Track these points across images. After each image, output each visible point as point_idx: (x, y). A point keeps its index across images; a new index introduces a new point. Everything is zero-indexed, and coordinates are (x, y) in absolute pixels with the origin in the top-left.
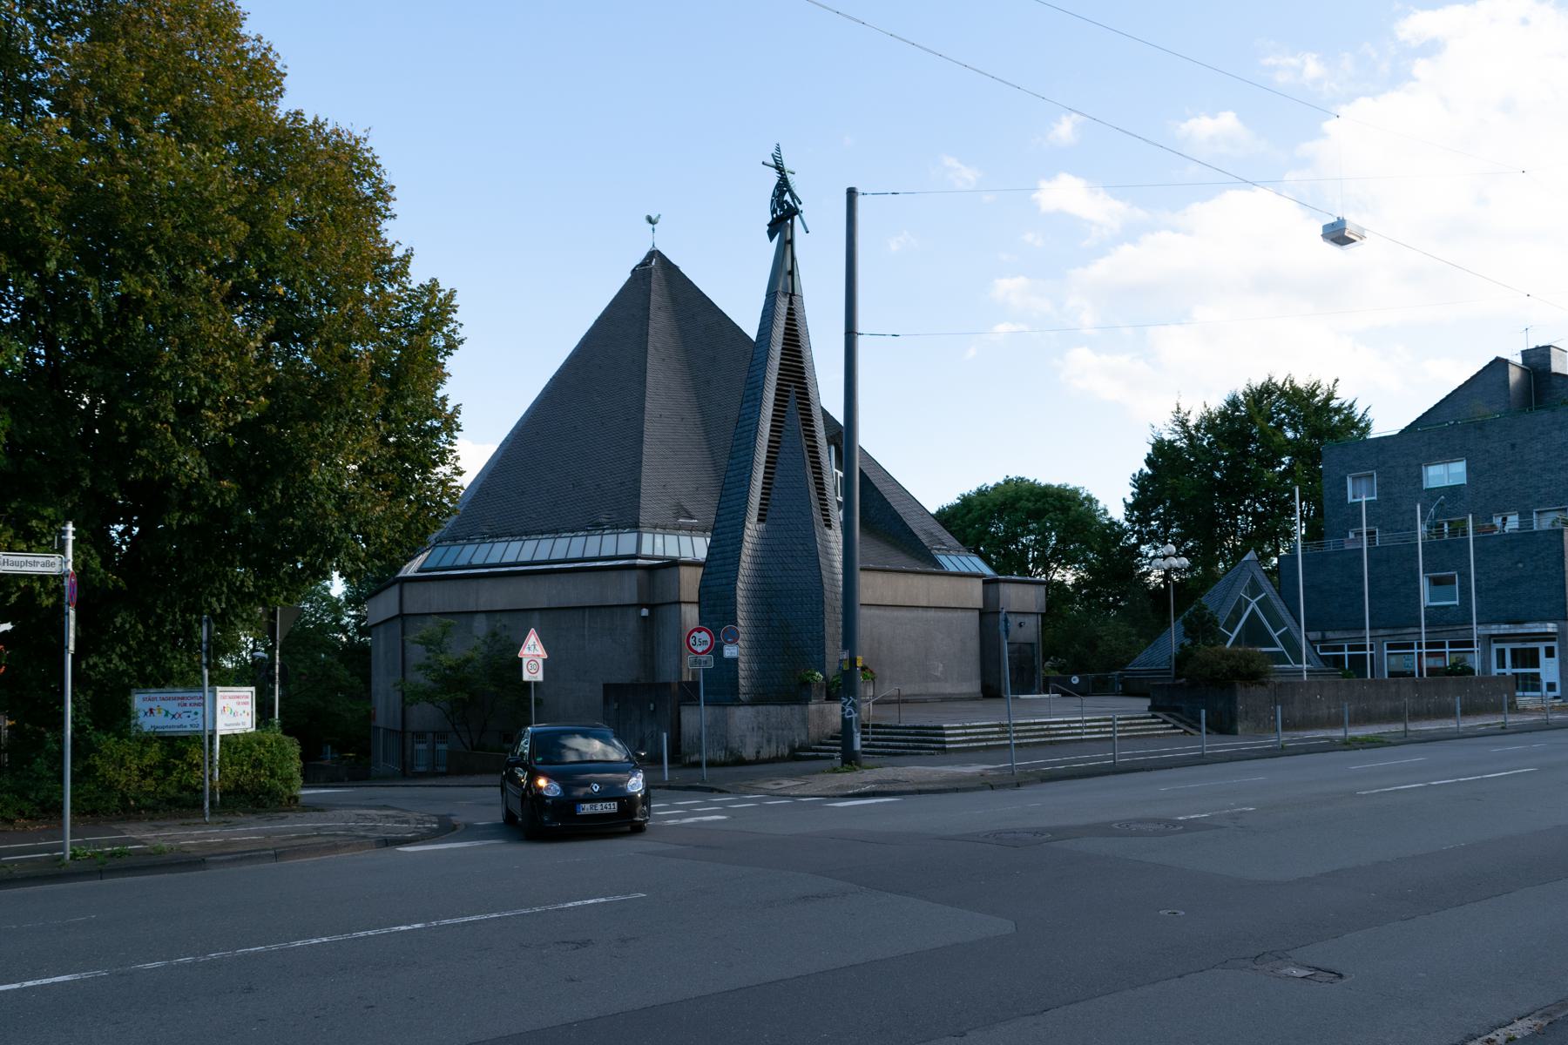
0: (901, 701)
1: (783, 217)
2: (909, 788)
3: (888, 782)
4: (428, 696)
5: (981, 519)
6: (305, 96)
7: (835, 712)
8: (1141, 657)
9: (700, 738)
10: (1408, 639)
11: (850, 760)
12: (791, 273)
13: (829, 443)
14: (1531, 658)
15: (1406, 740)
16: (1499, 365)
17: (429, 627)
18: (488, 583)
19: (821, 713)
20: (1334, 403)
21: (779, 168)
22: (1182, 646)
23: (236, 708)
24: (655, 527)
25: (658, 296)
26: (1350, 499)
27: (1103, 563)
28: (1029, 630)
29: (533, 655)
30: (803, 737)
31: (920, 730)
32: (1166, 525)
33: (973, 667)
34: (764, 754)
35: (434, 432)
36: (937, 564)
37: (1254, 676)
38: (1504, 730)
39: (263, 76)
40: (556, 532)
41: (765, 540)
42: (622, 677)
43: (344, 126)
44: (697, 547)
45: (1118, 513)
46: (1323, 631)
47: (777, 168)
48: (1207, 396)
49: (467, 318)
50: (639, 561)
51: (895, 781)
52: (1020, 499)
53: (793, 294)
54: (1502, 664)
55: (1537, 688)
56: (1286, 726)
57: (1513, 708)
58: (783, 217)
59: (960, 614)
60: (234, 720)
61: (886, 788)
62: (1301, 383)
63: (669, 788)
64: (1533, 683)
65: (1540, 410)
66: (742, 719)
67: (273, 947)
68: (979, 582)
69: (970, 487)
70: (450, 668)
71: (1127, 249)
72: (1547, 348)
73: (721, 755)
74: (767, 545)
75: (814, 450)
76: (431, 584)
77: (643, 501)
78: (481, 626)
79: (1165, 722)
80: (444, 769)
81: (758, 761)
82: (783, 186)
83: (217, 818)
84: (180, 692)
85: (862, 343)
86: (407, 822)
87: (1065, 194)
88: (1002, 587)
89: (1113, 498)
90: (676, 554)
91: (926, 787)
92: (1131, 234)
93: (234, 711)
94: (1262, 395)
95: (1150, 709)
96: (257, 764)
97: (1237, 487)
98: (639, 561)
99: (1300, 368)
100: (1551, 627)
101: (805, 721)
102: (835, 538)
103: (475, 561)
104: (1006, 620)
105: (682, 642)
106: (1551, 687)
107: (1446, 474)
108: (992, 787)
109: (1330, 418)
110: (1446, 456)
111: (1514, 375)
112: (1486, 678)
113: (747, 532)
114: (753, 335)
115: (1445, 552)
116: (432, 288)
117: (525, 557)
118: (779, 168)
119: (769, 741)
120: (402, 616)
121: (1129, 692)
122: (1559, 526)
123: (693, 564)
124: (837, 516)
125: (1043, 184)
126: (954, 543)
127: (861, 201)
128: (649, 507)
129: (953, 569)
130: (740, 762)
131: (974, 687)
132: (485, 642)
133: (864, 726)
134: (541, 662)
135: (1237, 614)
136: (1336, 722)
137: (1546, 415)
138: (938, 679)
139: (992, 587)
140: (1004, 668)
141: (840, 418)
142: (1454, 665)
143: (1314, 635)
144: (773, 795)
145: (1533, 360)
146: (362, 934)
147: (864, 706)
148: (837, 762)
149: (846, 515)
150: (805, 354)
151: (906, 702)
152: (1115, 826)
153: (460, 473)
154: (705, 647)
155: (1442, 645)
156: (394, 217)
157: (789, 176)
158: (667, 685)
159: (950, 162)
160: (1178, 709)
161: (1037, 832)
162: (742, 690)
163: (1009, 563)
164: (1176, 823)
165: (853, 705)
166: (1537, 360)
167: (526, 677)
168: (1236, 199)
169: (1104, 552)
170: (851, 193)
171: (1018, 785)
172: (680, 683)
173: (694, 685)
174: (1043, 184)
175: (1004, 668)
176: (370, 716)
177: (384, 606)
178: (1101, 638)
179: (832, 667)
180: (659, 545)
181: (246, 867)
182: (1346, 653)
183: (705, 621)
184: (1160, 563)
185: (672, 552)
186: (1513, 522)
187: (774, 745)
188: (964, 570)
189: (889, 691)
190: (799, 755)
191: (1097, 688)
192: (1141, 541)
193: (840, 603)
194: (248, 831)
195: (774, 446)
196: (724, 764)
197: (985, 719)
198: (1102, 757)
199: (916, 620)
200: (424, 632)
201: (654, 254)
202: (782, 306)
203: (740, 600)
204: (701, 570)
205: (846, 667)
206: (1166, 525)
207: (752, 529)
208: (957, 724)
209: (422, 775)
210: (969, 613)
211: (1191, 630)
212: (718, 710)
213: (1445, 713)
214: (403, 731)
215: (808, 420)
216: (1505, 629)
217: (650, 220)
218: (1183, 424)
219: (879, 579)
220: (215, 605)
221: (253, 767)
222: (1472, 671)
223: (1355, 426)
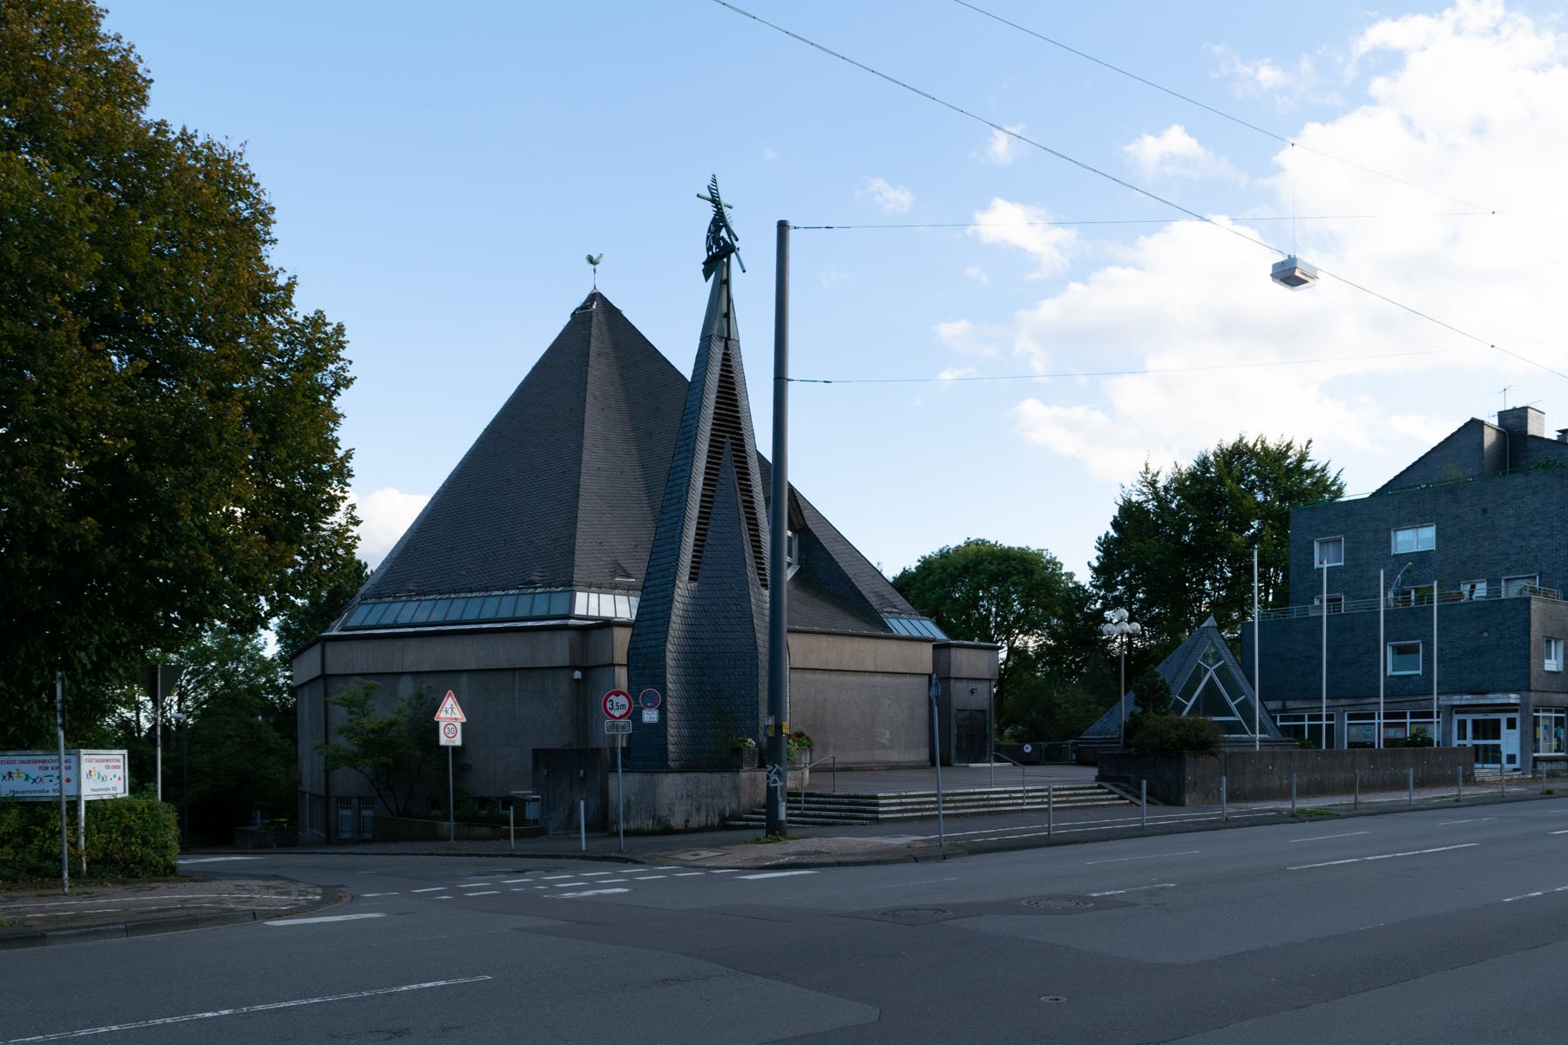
0: (831, 769)
2: (830, 860)
3: (810, 854)
4: (350, 760)
5: (942, 583)
6: (177, 104)
8: (1096, 726)
10: (1370, 709)
11: (775, 830)
12: (727, 315)
14: (1488, 729)
15: (1355, 812)
16: (1475, 426)
17: (354, 688)
18: (413, 643)
19: (753, 781)
20: (1307, 466)
21: (715, 201)
22: (1132, 714)
23: (104, 772)
24: (589, 587)
26: (1317, 565)
27: (1065, 628)
28: (983, 696)
29: (450, 719)
30: (734, 806)
32: (1132, 591)
34: (693, 824)
35: (324, 478)
36: (886, 627)
37: (1202, 745)
38: (1458, 803)
39: (124, 82)
42: (554, 742)
43: (217, 138)
45: (1084, 577)
46: (1284, 700)
47: (713, 201)
48: (1174, 458)
49: (356, 354)
50: (572, 622)
52: (981, 563)
53: (728, 338)
54: (1462, 736)
55: (1497, 760)
56: (1233, 797)
57: (1469, 780)
59: (908, 679)
60: (103, 785)
61: (806, 860)
62: (1272, 444)
63: (584, 858)
64: (1493, 755)
65: (1492, 466)
67: (53, 1037)
68: (929, 647)
69: (931, 549)
70: (373, 731)
71: (1075, 287)
72: (1525, 409)
73: (649, 824)
76: (354, 643)
77: (579, 558)
78: (406, 687)
79: (1111, 792)
80: (368, 836)
81: (686, 831)
82: (719, 221)
83: (77, 890)
84: (39, 755)
85: (792, 389)
86: (289, 894)
87: (1006, 222)
88: (955, 653)
89: (1078, 562)
92: (1081, 270)
93: (103, 775)
94: (1235, 457)
95: (1097, 779)
96: (127, 831)
97: (1203, 553)
98: (572, 622)
99: (1268, 425)
100: (1513, 698)
101: (736, 788)
103: (401, 620)
106: (1511, 759)
107: (1415, 540)
108: (916, 860)
109: (1302, 481)
110: (1415, 521)
111: (1489, 437)
112: (1446, 750)
113: (678, 591)
115: (1408, 622)
116: (317, 321)
118: (715, 201)
119: (698, 810)
120: (324, 677)
121: (1082, 762)
122: (1526, 594)
125: (978, 216)
127: (793, 236)
128: (583, 563)
129: (904, 633)
130: (668, 831)
131: (922, 755)
132: (410, 705)
135: (1196, 678)
136: (1284, 794)
137: (1518, 479)
138: (884, 747)
140: (958, 737)
142: (1415, 736)
143: (1272, 705)
144: (687, 866)
145: (1509, 422)
146: (158, 1022)
150: (742, 403)
152: (1024, 903)
153: (357, 523)
154: (623, 712)
155: (1403, 716)
156: (274, 241)
157: (725, 210)
158: (598, 751)
159: (879, 184)
160: (1126, 780)
161: (939, 909)
162: (671, 756)
163: (963, 625)
164: (1086, 900)
165: (778, 773)
166: (1514, 422)
167: (443, 741)
168: (1186, 228)
169: (1068, 618)
170: (783, 227)
174: (978, 216)
175: (958, 737)
176: (299, 782)
177: (309, 666)
178: (1058, 705)
180: (590, 604)
181: (92, 943)
182: (1306, 723)
184: (1119, 626)
186: (1481, 590)
187: (703, 814)
188: (916, 634)
189: (827, 759)
190: (728, 825)
191: (1052, 757)
192: (1106, 607)
194: (113, 900)
197: (920, 789)
198: (1036, 829)
200: (344, 694)
201: (595, 296)
202: (717, 351)
203: (670, 662)
205: (771, 734)
206: (1132, 591)
207: (683, 588)
208: (889, 795)
209: (345, 842)
210: (918, 680)
211: (1141, 700)
212: (646, 777)
213: (1399, 785)
214: (328, 796)
216: (1467, 699)
217: (591, 260)
218: (1153, 484)
220: (85, 660)
221: (123, 834)
222: (1430, 742)
223: (1326, 489)
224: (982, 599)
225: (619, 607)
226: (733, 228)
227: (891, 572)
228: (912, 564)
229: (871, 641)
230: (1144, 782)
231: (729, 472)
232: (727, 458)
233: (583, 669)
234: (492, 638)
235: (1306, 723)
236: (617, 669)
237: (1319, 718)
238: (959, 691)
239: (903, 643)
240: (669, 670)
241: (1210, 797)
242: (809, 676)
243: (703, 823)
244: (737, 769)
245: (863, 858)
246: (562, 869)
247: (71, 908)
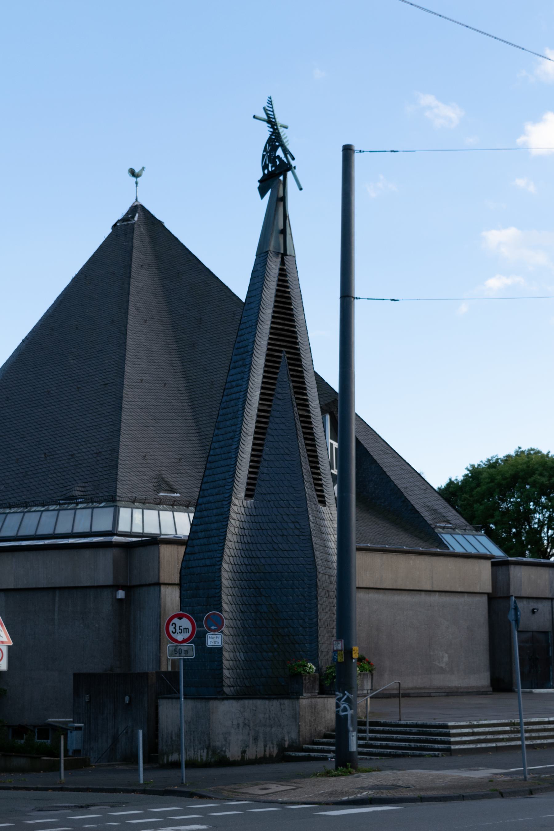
0: (402, 695)
1: (275, 173)
2: (410, 794)
3: (387, 788)
7: (328, 707)
9: (179, 736)
11: (345, 762)
12: (283, 232)
13: (324, 412)
19: (314, 709)
21: (271, 122)
25: (141, 252)
30: (294, 736)
31: (423, 729)
33: (482, 658)
34: (251, 754)
36: (441, 543)
40: (26, 505)
41: (251, 515)
42: (95, 665)
44: (180, 523)
50: (116, 539)
51: (395, 787)
53: (285, 254)
58: (275, 173)
59: (466, 599)
61: (385, 794)
63: (144, 792)
66: (227, 715)
68: (487, 565)
69: (480, 458)
73: (203, 755)
74: (255, 523)
75: (306, 421)
81: (243, 762)
82: (275, 141)
85: (359, 309)
90: (156, 531)
91: (430, 794)
98: (116, 539)
101: (296, 717)
102: (330, 514)
104: (516, 609)
105: (162, 631)
108: (502, 795)
113: (234, 508)
114: (243, 296)
117: (46, 529)
118: (271, 122)
119: (256, 739)
123: (175, 542)
124: (332, 491)
125: (529, 127)
126: (461, 521)
127: (357, 158)
128: (127, 478)
129: (459, 549)
130: (223, 762)
131: (482, 679)
133: (363, 723)
134: (5, 650)
138: (442, 671)
139: (501, 570)
141: (334, 383)
147: (361, 701)
148: (331, 765)
149: (340, 490)
150: (298, 318)
151: (407, 695)
154: (186, 636)
157: (281, 130)
158: (145, 675)
159: (428, 100)
162: (227, 681)
165: (348, 700)
170: (348, 151)
171: (531, 793)
172: (159, 674)
173: (174, 675)
174: (529, 127)
179: (325, 660)
183: (187, 607)
185: (152, 529)
187: (261, 744)
189: (388, 684)
190: (289, 756)
193: (334, 587)
195: (264, 415)
196: (206, 765)
197: (493, 717)
199: (416, 607)
201: (137, 208)
202: (274, 267)
203: (225, 582)
204: (182, 549)
205: (341, 659)
207: (239, 505)
208: (464, 722)
210: (477, 599)
212: (200, 704)
215: (300, 388)
217: (133, 173)
219: (378, 559)
224: (535, 511)
225: (178, 523)
226: (290, 147)
227: (438, 482)
228: (459, 474)
229: (427, 559)
231: (285, 388)
232: (284, 373)
233: (128, 589)
234: (31, 555)
236: (164, 590)
239: (460, 561)
240: (224, 590)
243: (260, 754)
244: (295, 695)
245: (446, 793)
246: (127, 805)
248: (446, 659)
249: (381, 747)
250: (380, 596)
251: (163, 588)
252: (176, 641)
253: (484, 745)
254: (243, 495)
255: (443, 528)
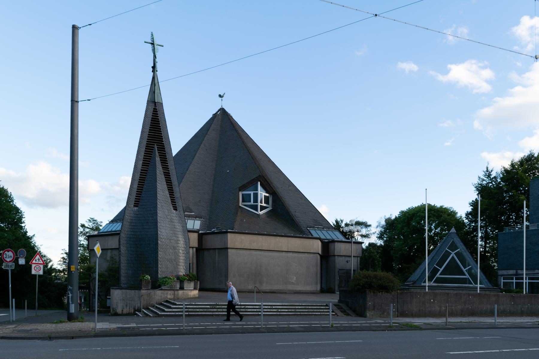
19: (149, 295)
34: (125, 312)
46: (517, 270)
81: (122, 315)
85: (82, 107)
87: (461, 73)
89: (462, 209)
119: (126, 306)
138: (293, 283)
154: (11, 259)
167: (33, 272)
187: (128, 308)
201: (222, 111)
217: (220, 96)
218: (489, 176)
229: (286, 238)
230: (26, 301)
235: (514, 281)
237: (522, 279)
238: (340, 263)
241: (384, 313)
242: (253, 252)
243: (128, 312)
244: (140, 288)
247: (376, 323)
248: (295, 278)
249: (308, 312)
250: (262, 253)
251: (336, 257)
252: (7, 261)
253: (194, 313)
254: (132, 206)
255: (318, 228)
